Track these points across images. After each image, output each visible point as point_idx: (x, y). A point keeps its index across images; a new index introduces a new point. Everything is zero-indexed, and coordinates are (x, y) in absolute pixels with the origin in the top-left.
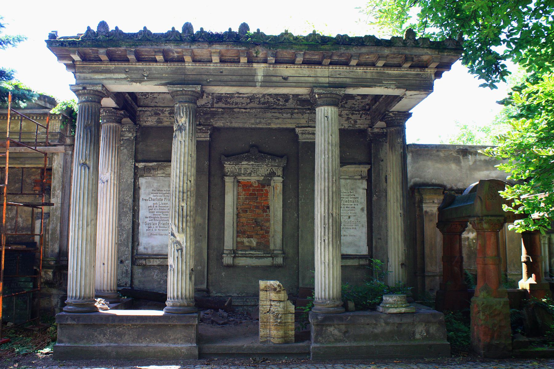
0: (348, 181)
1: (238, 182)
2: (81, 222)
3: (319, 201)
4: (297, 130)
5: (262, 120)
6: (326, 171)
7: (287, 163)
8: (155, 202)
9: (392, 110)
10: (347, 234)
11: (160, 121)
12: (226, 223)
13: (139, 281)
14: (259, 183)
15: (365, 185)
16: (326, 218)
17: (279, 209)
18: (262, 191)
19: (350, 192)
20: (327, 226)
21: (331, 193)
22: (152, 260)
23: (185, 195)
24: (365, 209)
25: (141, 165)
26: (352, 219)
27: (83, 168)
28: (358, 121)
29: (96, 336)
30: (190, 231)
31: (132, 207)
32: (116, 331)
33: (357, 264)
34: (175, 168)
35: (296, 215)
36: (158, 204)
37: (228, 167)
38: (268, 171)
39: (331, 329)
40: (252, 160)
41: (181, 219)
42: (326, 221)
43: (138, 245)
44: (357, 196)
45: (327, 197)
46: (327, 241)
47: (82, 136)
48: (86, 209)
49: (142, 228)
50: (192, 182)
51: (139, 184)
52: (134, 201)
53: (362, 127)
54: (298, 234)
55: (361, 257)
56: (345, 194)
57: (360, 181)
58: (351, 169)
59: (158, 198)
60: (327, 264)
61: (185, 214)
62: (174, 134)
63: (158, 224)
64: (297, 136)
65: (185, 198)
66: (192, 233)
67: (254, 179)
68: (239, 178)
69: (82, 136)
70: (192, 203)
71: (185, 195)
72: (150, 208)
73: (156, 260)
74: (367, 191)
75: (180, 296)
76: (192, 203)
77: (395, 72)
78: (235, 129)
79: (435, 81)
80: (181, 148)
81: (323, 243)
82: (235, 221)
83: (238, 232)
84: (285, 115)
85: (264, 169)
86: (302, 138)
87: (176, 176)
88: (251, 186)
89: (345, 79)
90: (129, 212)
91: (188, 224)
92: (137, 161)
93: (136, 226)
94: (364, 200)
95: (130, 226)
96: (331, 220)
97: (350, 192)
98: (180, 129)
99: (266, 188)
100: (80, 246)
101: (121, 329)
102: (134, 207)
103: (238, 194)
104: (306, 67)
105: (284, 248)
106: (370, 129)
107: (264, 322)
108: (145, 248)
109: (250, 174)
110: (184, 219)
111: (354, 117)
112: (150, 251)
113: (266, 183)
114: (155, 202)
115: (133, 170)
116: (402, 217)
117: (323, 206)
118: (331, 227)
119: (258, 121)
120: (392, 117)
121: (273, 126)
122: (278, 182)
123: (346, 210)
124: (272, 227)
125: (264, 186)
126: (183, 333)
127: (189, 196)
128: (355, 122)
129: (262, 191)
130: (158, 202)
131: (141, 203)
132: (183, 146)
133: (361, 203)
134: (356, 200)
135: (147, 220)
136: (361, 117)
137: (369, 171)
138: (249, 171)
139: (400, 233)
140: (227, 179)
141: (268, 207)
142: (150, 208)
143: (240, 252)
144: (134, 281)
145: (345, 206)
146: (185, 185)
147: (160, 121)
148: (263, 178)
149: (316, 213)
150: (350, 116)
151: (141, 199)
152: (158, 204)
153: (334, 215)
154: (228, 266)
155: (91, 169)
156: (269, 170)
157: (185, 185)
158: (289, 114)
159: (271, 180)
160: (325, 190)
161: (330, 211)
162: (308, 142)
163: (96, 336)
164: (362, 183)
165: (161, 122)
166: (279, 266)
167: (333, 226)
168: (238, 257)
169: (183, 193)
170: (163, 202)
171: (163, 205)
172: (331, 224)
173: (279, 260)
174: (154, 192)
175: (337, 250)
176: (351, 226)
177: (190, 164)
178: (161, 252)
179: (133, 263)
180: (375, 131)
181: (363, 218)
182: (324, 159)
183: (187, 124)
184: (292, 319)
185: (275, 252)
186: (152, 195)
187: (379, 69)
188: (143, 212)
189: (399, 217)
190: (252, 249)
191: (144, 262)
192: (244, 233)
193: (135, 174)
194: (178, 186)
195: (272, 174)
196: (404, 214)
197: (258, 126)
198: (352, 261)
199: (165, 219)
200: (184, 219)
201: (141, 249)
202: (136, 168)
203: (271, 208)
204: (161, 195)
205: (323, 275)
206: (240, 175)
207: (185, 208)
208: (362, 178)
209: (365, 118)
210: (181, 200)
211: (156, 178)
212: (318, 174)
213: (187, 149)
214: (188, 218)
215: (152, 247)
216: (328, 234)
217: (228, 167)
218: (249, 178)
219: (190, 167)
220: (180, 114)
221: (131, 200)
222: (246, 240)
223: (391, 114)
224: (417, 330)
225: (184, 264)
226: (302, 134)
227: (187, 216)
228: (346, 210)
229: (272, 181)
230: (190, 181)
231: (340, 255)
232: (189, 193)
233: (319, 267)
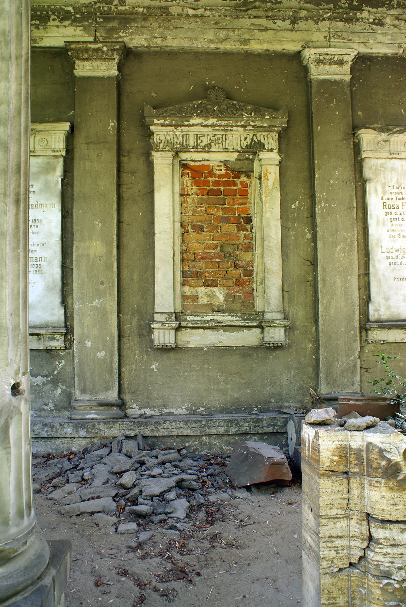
1: (184, 166)
5: (231, 34)
17: (272, 222)
18: (235, 184)
35: (309, 236)
38: (248, 141)
40: (213, 114)
64: (306, 69)
68: (184, 156)
83: (184, 274)
84: (279, 22)
88: (211, 173)
99: (243, 178)
119: (222, 34)
124: (258, 260)
129: (235, 184)
138: (205, 141)
141: (249, 220)
143: (190, 318)
154: (165, 350)
156: (249, 138)
158: (288, 22)
159: (252, 161)
166: (276, 347)
185: (268, 316)
192: (198, 274)
203: (256, 220)
206: (185, 148)
218: (205, 156)
222: (201, 291)
226: (319, 62)
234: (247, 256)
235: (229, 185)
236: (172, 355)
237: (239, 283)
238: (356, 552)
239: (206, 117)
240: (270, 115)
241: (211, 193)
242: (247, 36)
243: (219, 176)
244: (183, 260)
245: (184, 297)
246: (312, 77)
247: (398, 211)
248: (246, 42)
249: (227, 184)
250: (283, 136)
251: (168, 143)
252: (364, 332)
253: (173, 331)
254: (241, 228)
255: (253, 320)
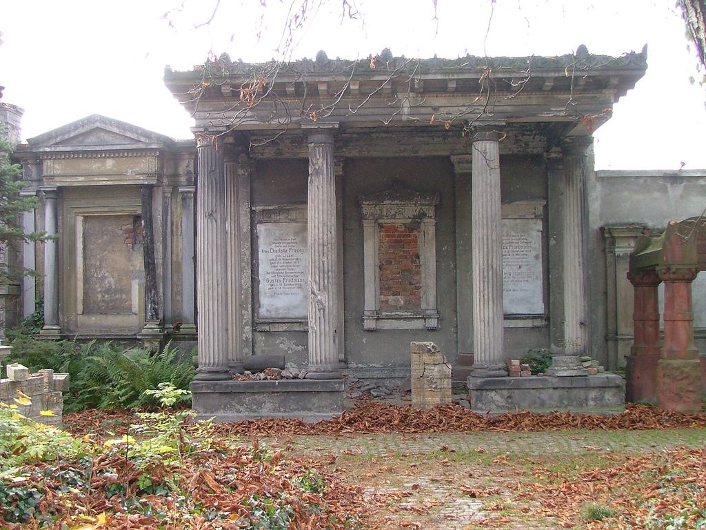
0: (518, 221)
1: (381, 226)
2: (211, 282)
3: (477, 251)
4: (452, 158)
5: (407, 147)
6: (485, 216)
7: (440, 202)
8: (278, 254)
9: (569, 134)
10: (517, 288)
11: (279, 152)
12: (660, 299)
13: (262, 351)
14: (406, 227)
15: (539, 225)
16: (486, 271)
17: (431, 259)
18: (410, 236)
19: (521, 236)
20: (486, 279)
21: (490, 242)
22: (276, 325)
23: (325, 248)
24: (541, 255)
25: (259, 208)
26: (523, 269)
27: (209, 220)
28: (530, 143)
29: (234, 406)
30: (332, 289)
31: (249, 261)
32: (255, 399)
33: (531, 325)
34: (313, 218)
35: (452, 266)
36: (282, 256)
37: (367, 208)
38: (417, 212)
39: (492, 394)
40: (397, 198)
41: (321, 275)
42: (486, 274)
43: (259, 307)
44: (529, 240)
45: (485, 247)
46: (486, 297)
47: (206, 184)
48: (215, 267)
49: (263, 286)
50: (333, 233)
51: (257, 233)
52: (252, 254)
53: (535, 151)
54: (456, 290)
55: (535, 317)
56: (514, 238)
57: (533, 221)
58: (522, 206)
59: (282, 248)
60: (486, 322)
61: (326, 269)
62: (309, 178)
63: (282, 281)
64: (452, 165)
65: (325, 251)
66: (334, 290)
67: (398, 222)
68: (381, 221)
69: (206, 184)
70: (333, 256)
71: (325, 248)
72: (272, 261)
73: (281, 325)
74: (542, 234)
75: (324, 360)
76: (333, 256)
77: (564, 96)
78: (373, 159)
79: (614, 105)
80: (319, 195)
81: (482, 298)
82: (377, 274)
83: (381, 289)
84: (436, 139)
85: (411, 210)
86: (459, 169)
87: (315, 227)
88: (396, 230)
89: (505, 107)
90: (246, 267)
91: (330, 280)
92: (252, 203)
93: (255, 284)
94: (539, 245)
95: (249, 284)
96: (490, 273)
97: (521, 236)
98: (317, 173)
99: (415, 232)
100: (211, 308)
101: (260, 397)
102: (252, 261)
103: (381, 241)
104: (460, 95)
105: (439, 307)
106: (545, 154)
107: (417, 388)
108: (267, 311)
109: (395, 215)
110: (326, 276)
111: (526, 138)
112: (273, 315)
113: (415, 225)
114: (278, 254)
115: (249, 215)
116: (581, 266)
117: (481, 256)
118: (491, 281)
119: (402, 148)
120: (569, 143)
121: (421, 154)
122: (429, 227)
123: (516, 259)
124: (423, 280)
125: (412, 230)
126: (329, 401)
127: (330, 249)
128: (527, 144)
129: (410, 236)
130: (281, 254)
131: (261, 256)
132: (321, 193)
133: (535, 249)
134: (529, 245)
135: (269, 276)
136: (534, 138)
137: (546, 207)
138: (393, 212)
139: (578, 284)
140: (365, 223)
141: (418, 257)
142: (272, 261)
143: (384, 313)
144: (255, 350)
145: (515, 253)
146: (325, 236)
147: (279, 152)
148: (410, 220)
149: (474, 264)
150: (520, 137)
151: (260, 250)
152: (282, 256)
153: (494, 267)
154: (370, 331)
155: (219, 221)
156: (418, 210)
157: (325, 236)
158: (441, 139)
159: (420, 223)
160: (483, 238)
161: (490, 262)
162: (466, 173)
163: (234, 406)
164: (535, 224)
165: (281, 154)
166: (433, 330)
167: (492, 279)
168: (383, 319)
169: (323, 245)
170: (287, 254)
171: (288, 258)
172: (490, 277)
173: (433, 323)
174: (276, 242)
175: (499, 306)
176: (522, 278)
177: (329, 212)
178: (287, 316)
179: (254, 331)
180: (553, 156)
181: (539, 268)
182: (482, 203)
183: (325, 167)
184: (448, 385)
185: (428, 312)
186: (274, 245)
187: (546, 93)
188: (263, 268)
189: (577, 266)
190: (397, 308)
191: (267, 328)
192: (389, 289)
193: (252, 219)
194: (317, 238)
195: (422, 215)
196: (583, 264)
197: (402, 155)
198: (523, 321)
199: (291, 275)
200: (326, 276)
201: (263, 312)
202: (252, 212)
203: (422, 258)
204: (285, 245)
205: (483, 334)
206: (381, 217)
207: (326, 263)
208: (536, 217)
209: (538, 139)
210: (321, 254)
211: (277, 225)
212: (476, 220)
213: (325, 195)
214: (330, 273)
215: (277, 309)
216: (488, 288)
217: (367, 208)
218: (393, 221)
219: (329, 216)
220: (316, 156)
221: (248, 253)
222: (391, 298)
223: (567, 140)
224: (590, 396)
225: (327, 324)
226: (459, 163)
227: (328, 271)
228: (516, 259)
229: (422, 224)
230: (331, 232)
231: (502, 313)
232: (329, 245)
233: (478, 326)
234: (417, 278)
235: (407, 237)
236: (374, 333)
237: (413, 294)
238: (509, 501)
239: (393, 200)
240: (430, 197)
241: (396, 241)
242: (417, 149)
243: (401, 232)
244: (380, 280)
245: (382, 302)
246: (455, 171)
247: (507, 250)
248: (417, 152)
249: (405, 236)
250: (438, 208)
251: (372, 214)
252: (610, 343)
253: (374, 321)
254: (413, 262)
255: (419, 314)
